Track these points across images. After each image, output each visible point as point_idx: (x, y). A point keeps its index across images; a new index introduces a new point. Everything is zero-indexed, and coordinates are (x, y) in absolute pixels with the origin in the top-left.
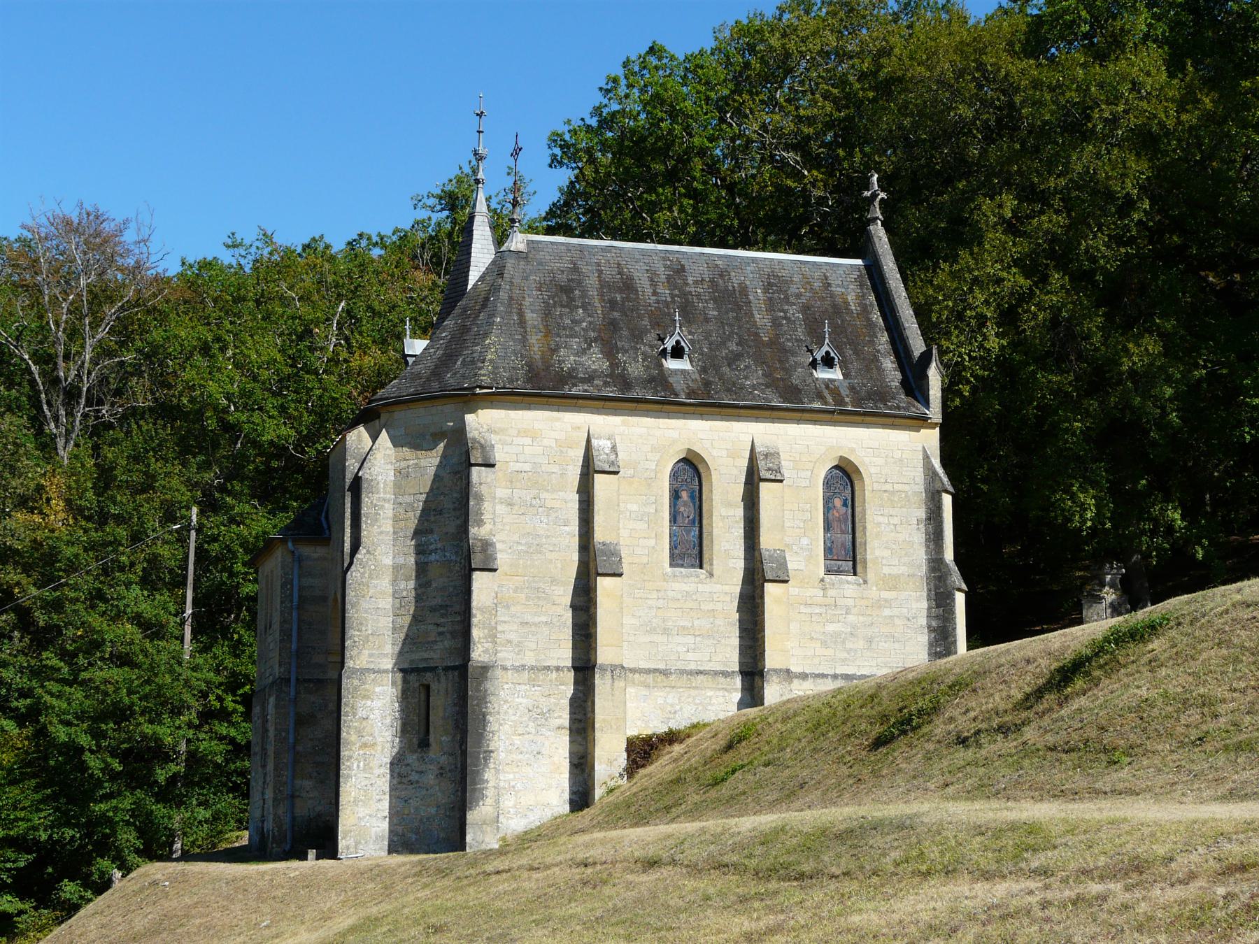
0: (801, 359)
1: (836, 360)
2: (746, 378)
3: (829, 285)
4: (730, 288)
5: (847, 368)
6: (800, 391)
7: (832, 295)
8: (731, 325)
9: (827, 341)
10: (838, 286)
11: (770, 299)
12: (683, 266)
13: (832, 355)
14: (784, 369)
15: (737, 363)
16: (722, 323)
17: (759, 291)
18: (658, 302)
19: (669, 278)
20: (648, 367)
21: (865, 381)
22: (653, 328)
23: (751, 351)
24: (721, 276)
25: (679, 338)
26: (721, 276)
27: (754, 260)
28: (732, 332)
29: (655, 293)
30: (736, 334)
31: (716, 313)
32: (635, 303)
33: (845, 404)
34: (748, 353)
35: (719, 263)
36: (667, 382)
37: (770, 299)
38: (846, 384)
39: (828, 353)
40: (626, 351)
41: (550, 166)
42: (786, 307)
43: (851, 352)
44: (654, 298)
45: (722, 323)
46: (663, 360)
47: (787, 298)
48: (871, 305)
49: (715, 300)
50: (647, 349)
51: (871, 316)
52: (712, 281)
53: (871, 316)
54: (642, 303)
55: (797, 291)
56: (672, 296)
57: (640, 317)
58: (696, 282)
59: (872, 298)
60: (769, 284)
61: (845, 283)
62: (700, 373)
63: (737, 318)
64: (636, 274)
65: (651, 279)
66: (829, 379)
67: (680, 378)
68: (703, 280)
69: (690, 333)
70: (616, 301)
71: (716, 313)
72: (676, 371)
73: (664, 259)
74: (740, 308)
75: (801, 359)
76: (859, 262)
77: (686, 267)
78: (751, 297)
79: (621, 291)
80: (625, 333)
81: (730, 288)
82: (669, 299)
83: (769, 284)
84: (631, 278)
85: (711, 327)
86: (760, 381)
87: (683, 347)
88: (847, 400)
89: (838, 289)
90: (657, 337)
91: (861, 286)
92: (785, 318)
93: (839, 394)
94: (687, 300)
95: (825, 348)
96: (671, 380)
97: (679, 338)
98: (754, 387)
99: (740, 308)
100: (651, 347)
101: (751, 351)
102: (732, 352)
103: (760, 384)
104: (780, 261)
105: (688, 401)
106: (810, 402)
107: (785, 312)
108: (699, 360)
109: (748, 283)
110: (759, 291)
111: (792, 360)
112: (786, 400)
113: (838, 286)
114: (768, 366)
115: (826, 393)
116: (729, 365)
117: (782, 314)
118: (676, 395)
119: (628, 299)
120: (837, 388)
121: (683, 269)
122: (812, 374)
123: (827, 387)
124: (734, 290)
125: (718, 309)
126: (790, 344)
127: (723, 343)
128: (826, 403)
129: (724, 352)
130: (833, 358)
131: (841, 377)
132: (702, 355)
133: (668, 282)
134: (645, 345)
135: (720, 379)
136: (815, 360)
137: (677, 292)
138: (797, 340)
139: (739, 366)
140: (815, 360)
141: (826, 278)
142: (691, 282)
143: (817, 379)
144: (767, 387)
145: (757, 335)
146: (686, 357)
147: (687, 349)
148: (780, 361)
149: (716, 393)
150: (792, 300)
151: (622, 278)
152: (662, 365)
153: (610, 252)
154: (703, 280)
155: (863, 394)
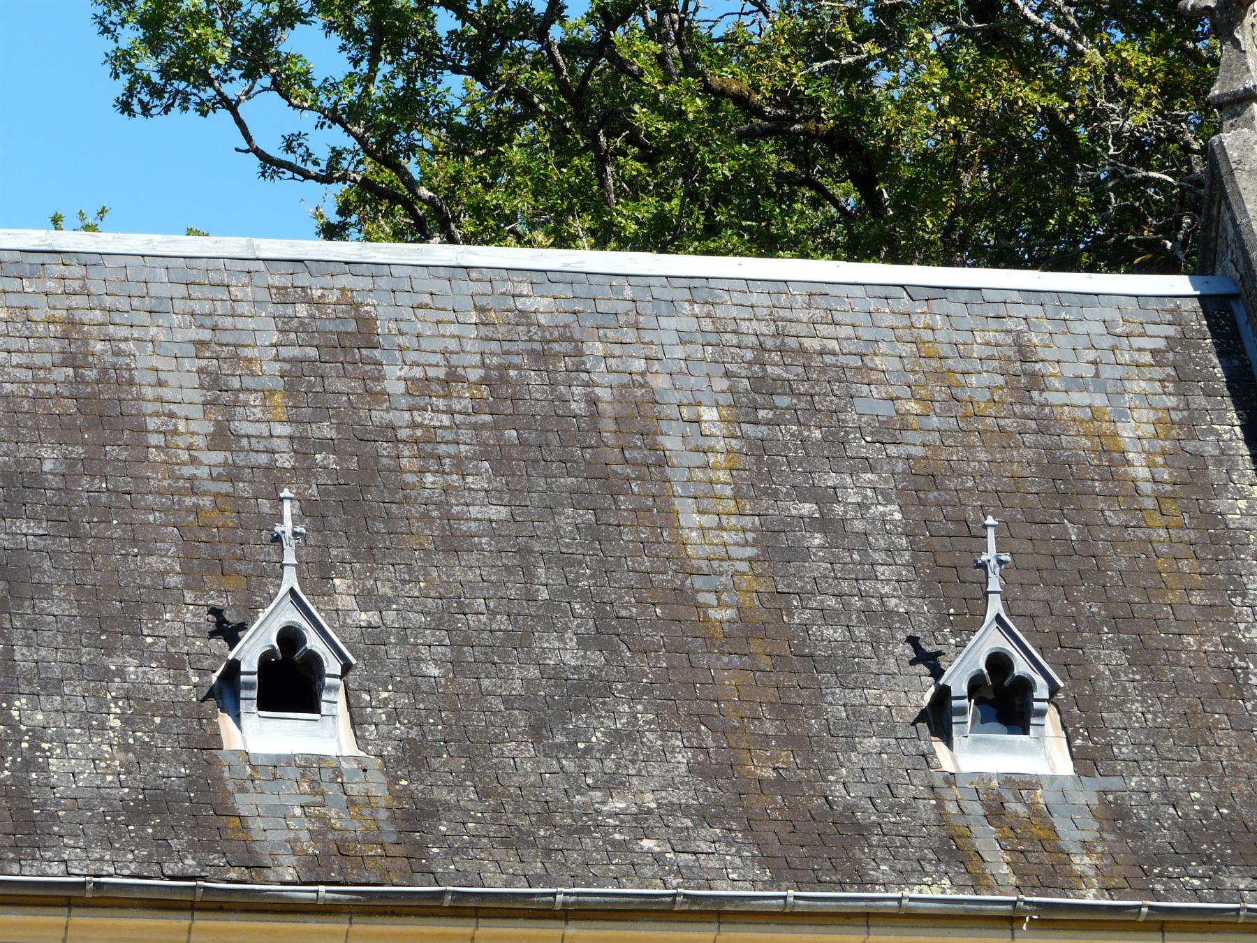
0: (882, 697)
1: (1042, 690)
2: (612, 784)
3: (1037, 382)
4: (578, 407)
5: (1093, 727)
6: (861, 832)
7: (1046, 424)
8: (564, 561)
9: (995, 606)
10: (1077, 382)
11: (759, 448)
12: (366, 325)
13: (1021, 667)
14: (799, 742)
15: (579, 721)
16: (524, 552)
17: (709, 414)
18: (232, 474)
19: (294, 374)
20: (146, 752)
21: (1177, 783)
22: (199, 588)
23: (649, 669)
24: (541, 357)
25: (291, 616)
26: (541, 357)
27: (695, 287)
28: (569, 591)
29: (222, 438)
30: (586, 596)
31: (498, 512)
32: (124, 483)
33: (1073, 881)
34: (632, 677)
35: (536, 303)
36: (224, 810)
37: (759, 448)
38: (1086, 796)
39: (999, 662)
40: (53, 686)
41: (125, 107)
42: (832, 480)
43: (1117, 658)
44: (217, 457)
45: (524, 552)
46: (225, 721)
47: (836, 440)
48: (1224, 457)
49: (500, 460)
50: (158, 676)
51: (1221, 504)
52: (495, 380)
53: (1221, 504)
54: (157, 479)
55: (886, 410)
56: (303, 447)
57: (142, 540)
58: (419, 388)
59: (1230, 427)
60: (762, 385)
61: (1107, 372)
62: (389, 768)
63: (595, 534)
64: (144, 361)
65: (213, 381)
66: (1009, 780)
67: (293, 796)
68: (453, 377)
69: (367, 599)
70: (38, 476)
71: (498, 512)
72: (276, 766)
73: (283, 295)
74: (612, 487)
75: (882, 697)
76: (1181, 284)
77: (382, 327)
78: (670, 443)
79: (64, 431)
80: (59, 606)
81: (578, 407)
82: (285, 461)
83: (762, 385)
84: (120, 378)
85: (467, 570)
86: (674, 797)
87: (314, 660)
88: (1082, 863)
89: (1077, 397)
90: (207, 621)
91: (1182, 381)
92: (822, 523)
93: (1050, 842)
94: (370, 467)
95: (989, 640)
96: (243, 803)
97: (291, 616)
98: (641, 821)
99: (612, 487)
100: (174, 663)
101: (649, 669)
102: (556, 675)
103: (673, 809)
104: (816, 292)
105: (305, 893)
106: (903, 879)
107: (826, 497)
108: (395, 715)
109: (660, 382)
110: (709, 414)
111: (837, 703)
112: (784, 871)
113: (1077, 382)
114: (721, 732)
115: (987, 841)
116: (536, 732)
117: (808, 508)
118: (256, 867)
119: (94, 465)
120: (1041, 815)
121: (366, 332)
122: (927, 757)
123: (996, 812)
124: (596, 415)
125: (514, 496)
126: (835, 633)
127: (519, 640)
128: (978, 882)
129: (520, 676)
130: (1025, 685)
131: (1064, 766)
132: (415, 691)
133: (290, 390)
134: (144, 656)
135: (483, 794)
136: (943, 694)
137: (326, 430)
138: (869, 616)
139: (577, 734)
140: (943, 694)
141: (1024, 352)
142: (394, 386)
143: (951, 779)
144: (704, 817)
145: (684, 596)
146: (335, 702)
147: (332, 666)
148: (784, 710)
149: (452, 852)
150: (859, 446)
151: (79, 380)
152: (213, 742)
153: (36, 273)
154: (453, 377)
155: (1164, 837)
